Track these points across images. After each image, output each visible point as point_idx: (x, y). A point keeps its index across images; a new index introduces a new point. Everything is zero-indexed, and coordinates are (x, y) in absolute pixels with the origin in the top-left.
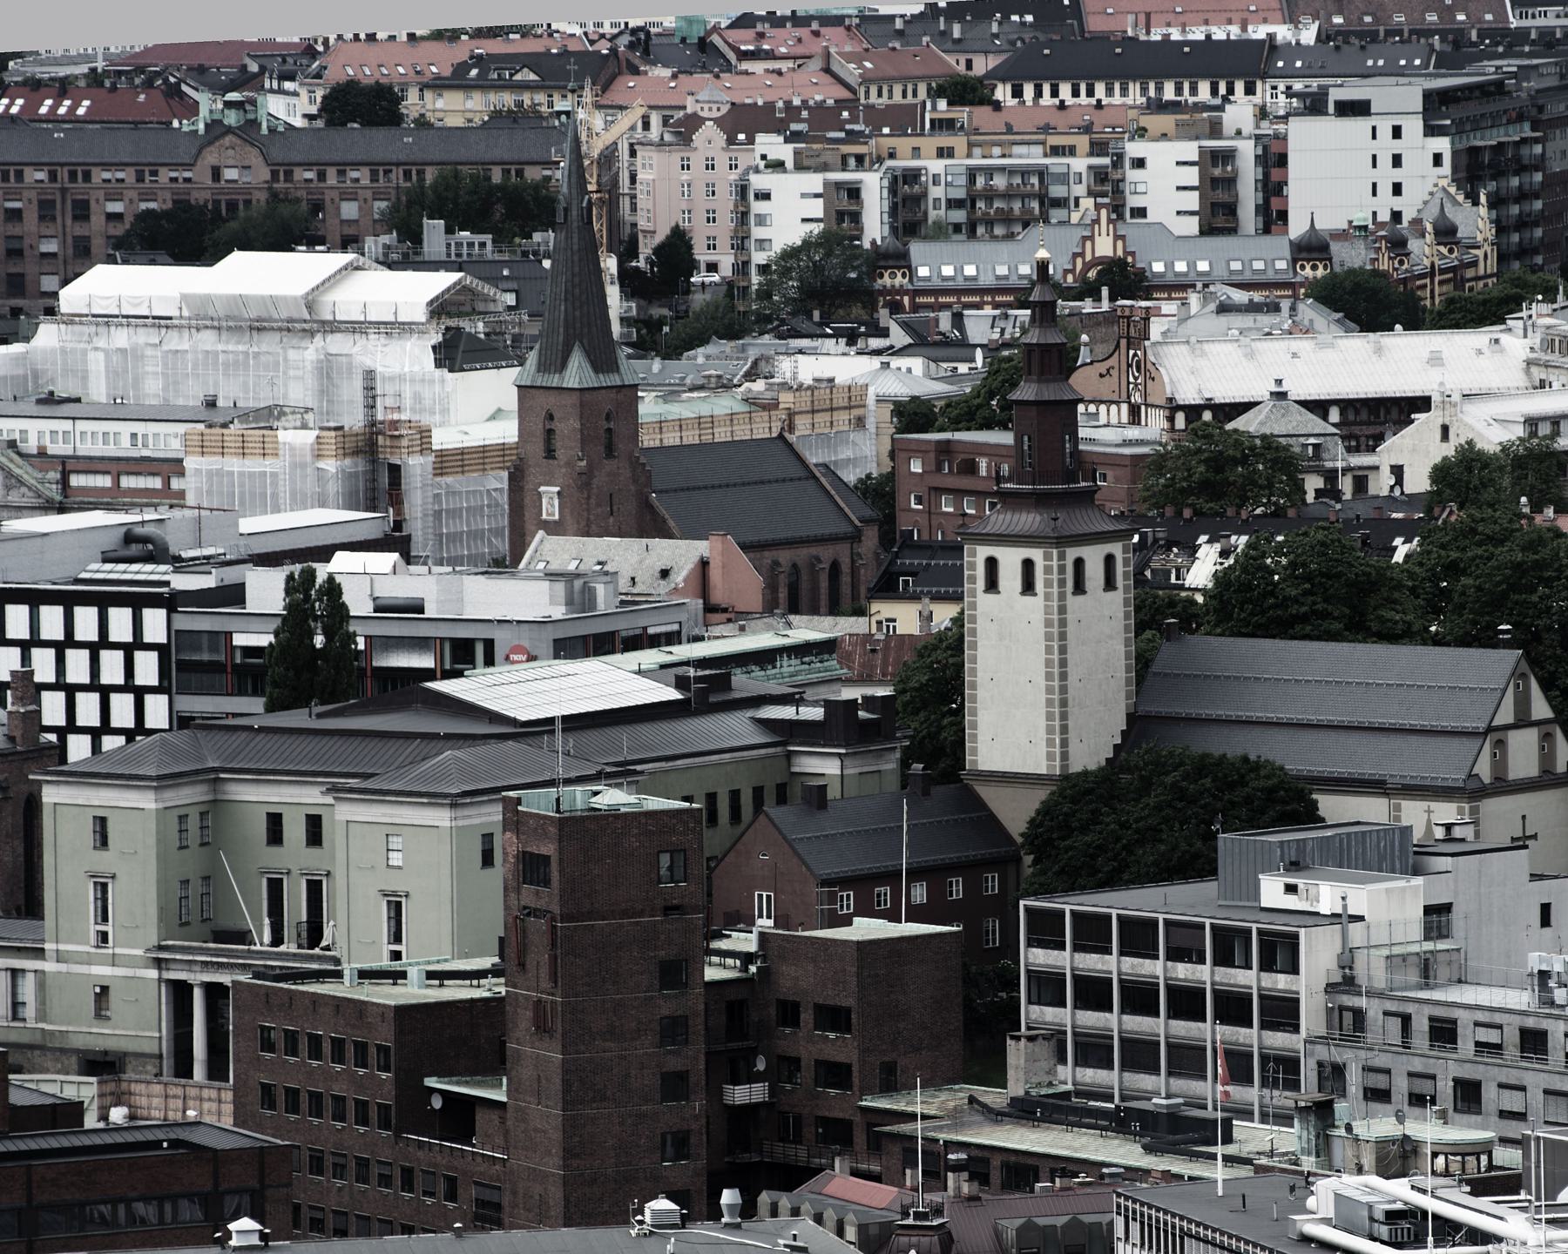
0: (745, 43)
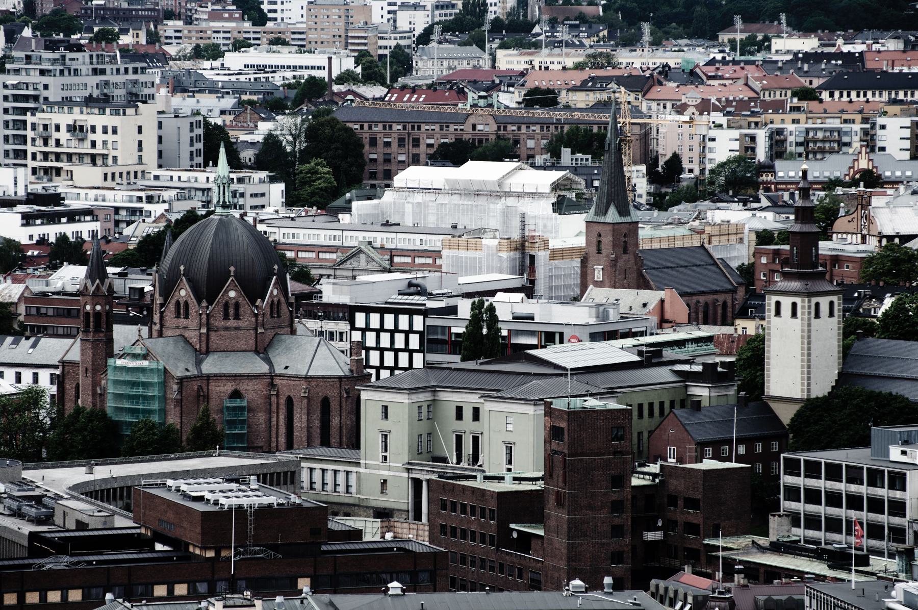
0: (711, 72)
